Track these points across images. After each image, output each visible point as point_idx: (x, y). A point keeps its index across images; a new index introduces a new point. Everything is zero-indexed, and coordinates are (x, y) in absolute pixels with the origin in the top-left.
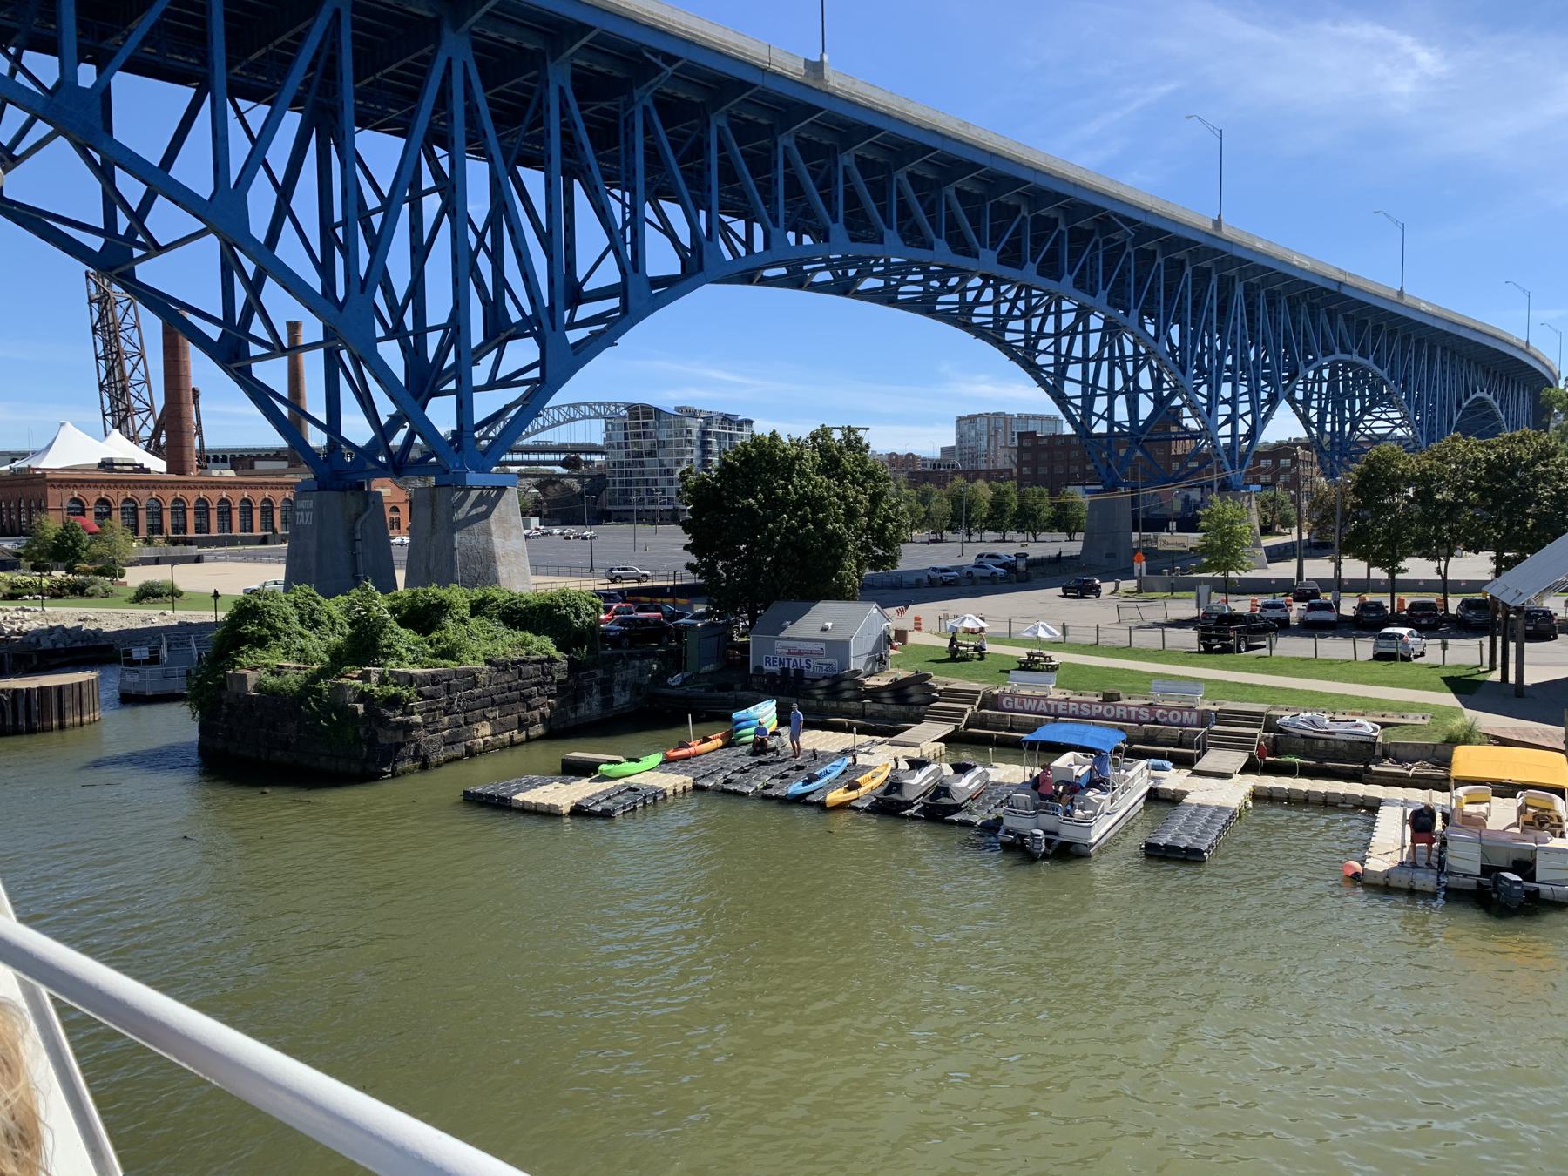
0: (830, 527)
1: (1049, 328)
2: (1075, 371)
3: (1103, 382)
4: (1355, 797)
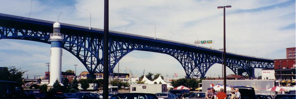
0: (16, 73)
1: (184, 58)
2: (183, 60)
3: (187, 62)
4: (241, 79)
